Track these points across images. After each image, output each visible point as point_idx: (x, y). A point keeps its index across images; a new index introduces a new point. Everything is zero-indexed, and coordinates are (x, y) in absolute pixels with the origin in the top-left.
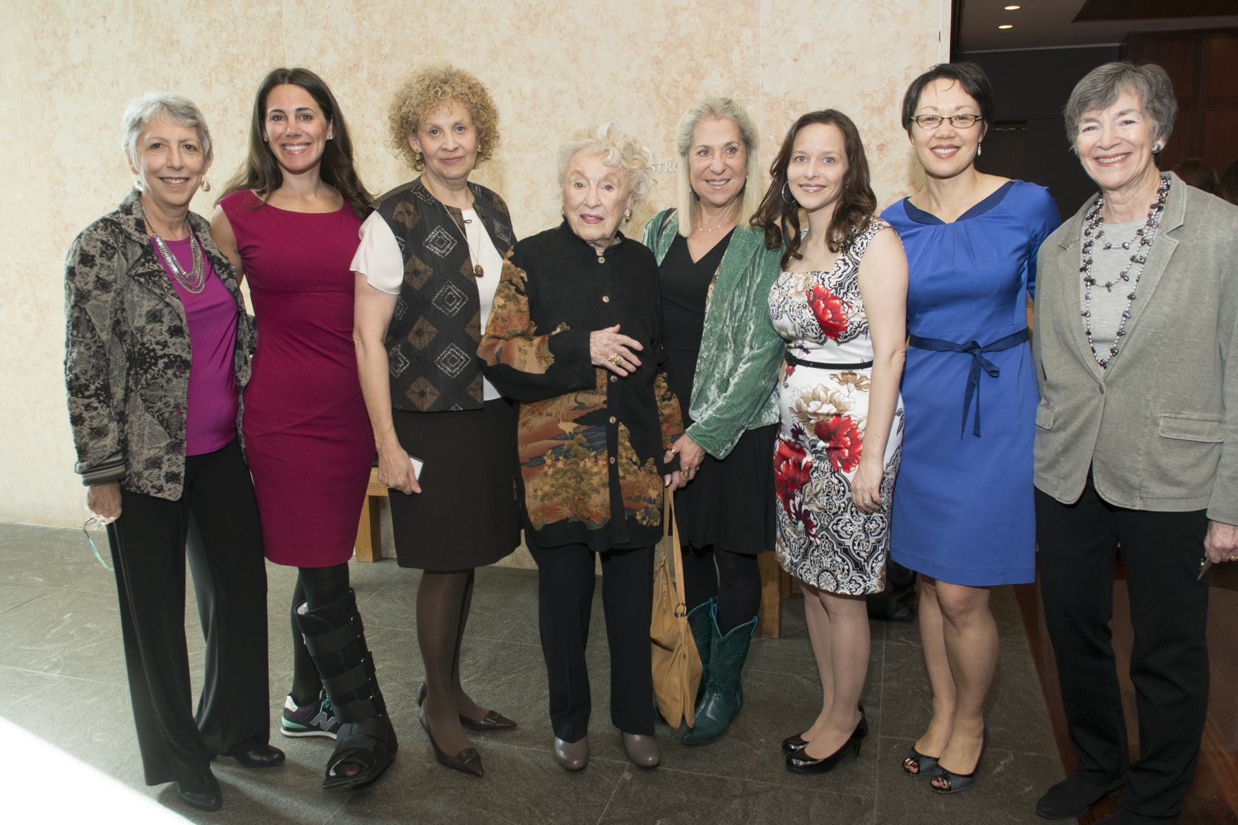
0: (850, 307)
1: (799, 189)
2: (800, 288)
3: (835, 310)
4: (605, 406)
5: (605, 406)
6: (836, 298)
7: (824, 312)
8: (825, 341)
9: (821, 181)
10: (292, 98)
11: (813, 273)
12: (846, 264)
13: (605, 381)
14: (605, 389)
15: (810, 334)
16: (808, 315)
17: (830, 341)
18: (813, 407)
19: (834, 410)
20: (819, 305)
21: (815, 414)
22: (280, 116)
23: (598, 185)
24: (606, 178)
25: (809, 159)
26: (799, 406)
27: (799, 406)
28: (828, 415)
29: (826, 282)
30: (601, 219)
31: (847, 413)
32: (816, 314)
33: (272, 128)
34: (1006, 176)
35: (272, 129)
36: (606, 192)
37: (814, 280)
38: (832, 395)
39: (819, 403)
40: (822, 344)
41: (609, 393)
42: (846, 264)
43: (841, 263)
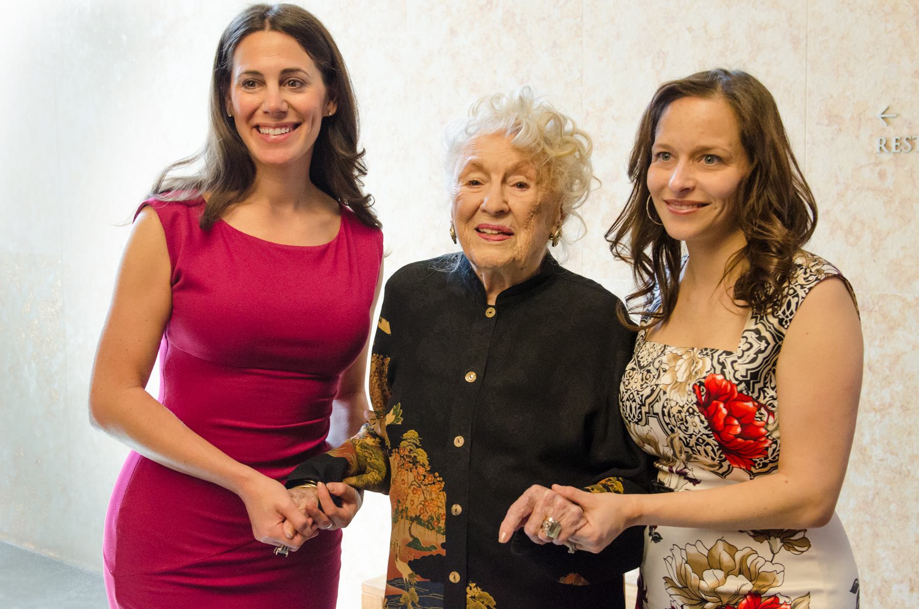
0: (771, 413)
1: (664, 204)
2: (681, 377)
3: (747, 419)
4: (443, 552)
5: (443, 552)
6: (748, 399)
7: (728, 424)
8: (729, 471)
9: (695, 197)
10: (273, 51)
11: (704, 351)
12: (760, 338)
13: (443, 511)
14: (442, 524)
15: (702, 458)
16: (698, 424)
17: (738, 472)
18: (710, 580)
19: (748, 587)
20: (718, 410)
21: (714, 592)
22: (254, 81)
23: (504, 181)
24: (516, 170)
25: (676, 157)
26: (683, 577)
27: (683, 577)
28: (737, 594)
29: (728, 369)
30: (510, 234)
31: (772, 591)
32: (711, 425)
33: (241, 99)
34: (330, 403)
35: (241, 99)
36: (517, 191)
37: (705, 366)
38: (744, 559)
39: (720, 574)
40: (723, 475)
41: (448, 532)
42: (760, 338)
43: (752, 337)
